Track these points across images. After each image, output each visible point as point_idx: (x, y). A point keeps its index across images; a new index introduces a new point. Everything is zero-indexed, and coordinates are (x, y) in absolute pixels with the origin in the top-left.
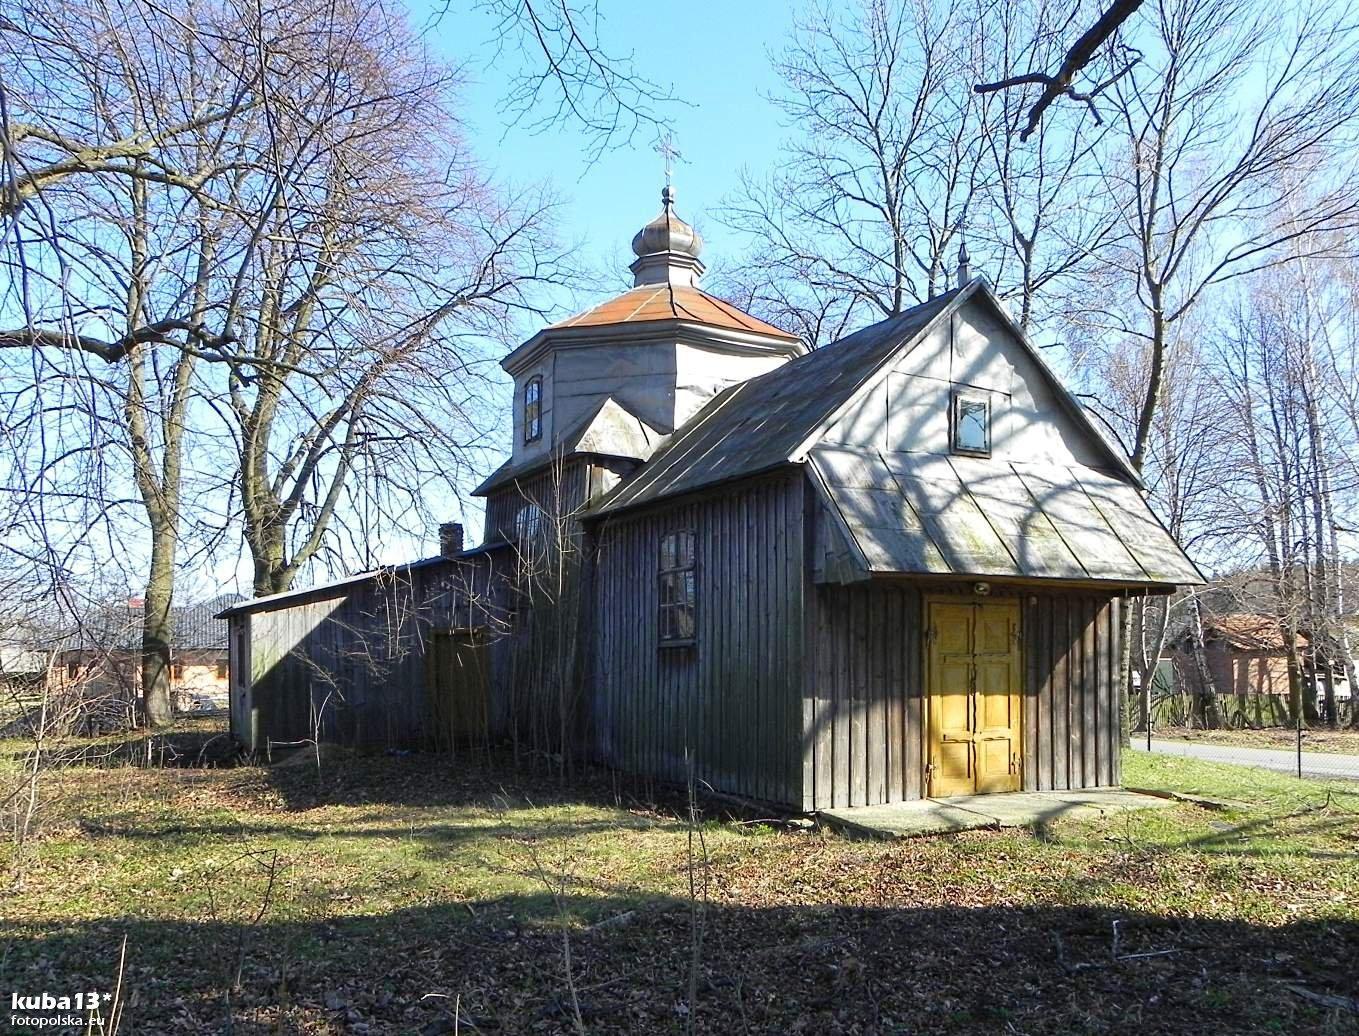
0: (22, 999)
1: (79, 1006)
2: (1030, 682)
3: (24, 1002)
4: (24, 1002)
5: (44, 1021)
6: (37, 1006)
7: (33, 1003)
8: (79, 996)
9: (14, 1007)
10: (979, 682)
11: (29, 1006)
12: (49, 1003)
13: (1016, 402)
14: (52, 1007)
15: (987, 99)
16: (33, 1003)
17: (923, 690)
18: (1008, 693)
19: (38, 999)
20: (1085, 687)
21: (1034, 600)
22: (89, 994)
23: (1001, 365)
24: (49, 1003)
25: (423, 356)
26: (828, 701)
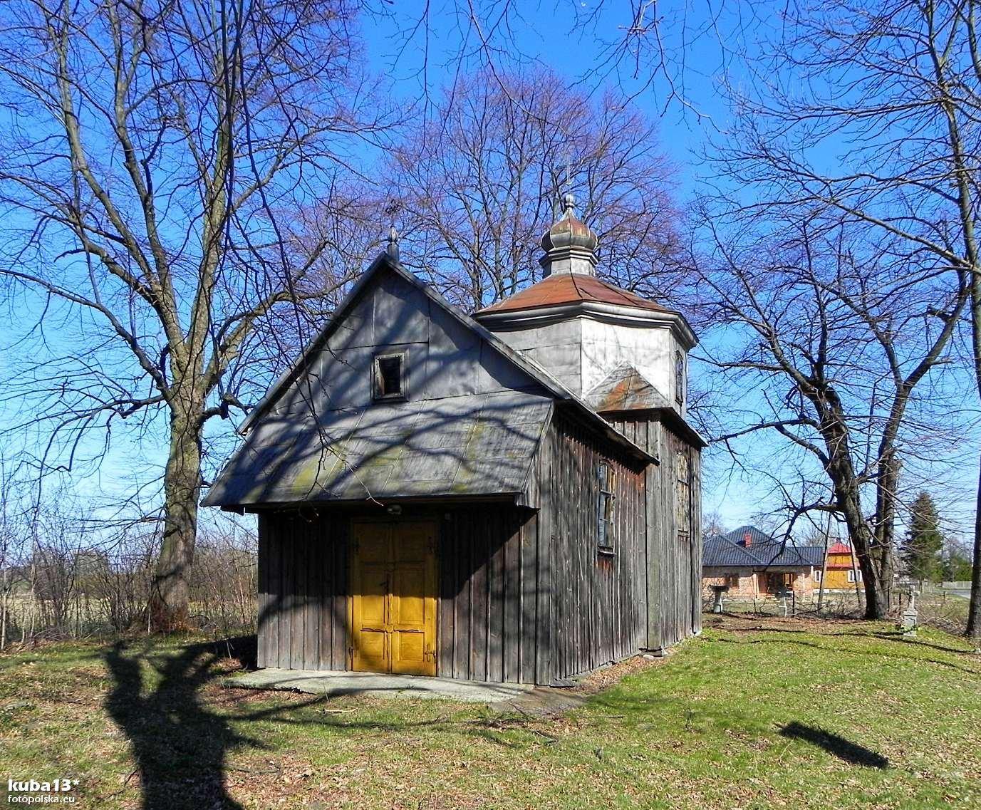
0: (16, 783)
1: (56, 789)
2: (447, 589)
3: (17, 786)
4: (17, 786)
5: (31, 800)
6: (26, 789)
7: (23, 786)
8: (56, 782)
9: (10, 789)
10: (390, 587)
11: (21, 789)
12: (35, 786)
13: (433, 350)
14: (37, 789)
15: (162, 5)
16: (23, 786)
17: (346, 591)
18: (436, 598)
19: (27, 784)
20: (507, 595)
21: (448, 516)
22: (64, 780)
23: (418, 323)
24: (35, 786)
25: (899, 489)
26: (276, 596)
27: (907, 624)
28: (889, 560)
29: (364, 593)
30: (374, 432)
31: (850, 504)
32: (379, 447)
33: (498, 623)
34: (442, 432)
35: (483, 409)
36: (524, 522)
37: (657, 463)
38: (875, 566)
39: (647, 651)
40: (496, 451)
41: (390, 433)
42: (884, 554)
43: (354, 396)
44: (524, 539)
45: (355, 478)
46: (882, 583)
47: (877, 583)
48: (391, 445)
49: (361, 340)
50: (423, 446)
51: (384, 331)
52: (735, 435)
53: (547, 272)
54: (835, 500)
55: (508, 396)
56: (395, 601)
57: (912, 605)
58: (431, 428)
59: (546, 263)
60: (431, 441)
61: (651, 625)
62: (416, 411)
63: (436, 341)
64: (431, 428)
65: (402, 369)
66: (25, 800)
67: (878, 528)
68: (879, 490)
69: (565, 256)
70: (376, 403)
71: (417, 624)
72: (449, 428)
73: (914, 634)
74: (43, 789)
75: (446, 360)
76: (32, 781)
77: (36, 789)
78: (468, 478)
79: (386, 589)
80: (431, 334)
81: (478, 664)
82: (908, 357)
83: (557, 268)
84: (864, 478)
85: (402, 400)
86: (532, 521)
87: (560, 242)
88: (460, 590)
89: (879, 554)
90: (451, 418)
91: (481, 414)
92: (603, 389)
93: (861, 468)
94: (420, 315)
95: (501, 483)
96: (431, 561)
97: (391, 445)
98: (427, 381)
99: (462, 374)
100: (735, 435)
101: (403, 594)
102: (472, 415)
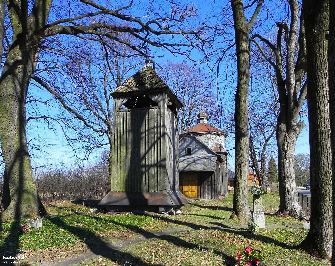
3: (6, 258)
4: (6, 258)
5: (11, 262)
9: (3, 259)
11: (7, 259)
12: (12, 258)
16: (8, 258)
19: (9, 257)
24: (12, 258)
27: (268, 191)
28: (264, 178)
29: (184, 185)
30: (188, 160)
31: (256, 166)
32: (190, 163)
33: (208, 189)
34: (200, 161)
35: (206, 157)
36: (212, 174)
37: (224, 162)
38: (261, 179)
39: (223, 196)
40: (210, 164)
41: (191, 160)
42: (263, 177)
43: (183, 154)
44: (213, 177)
45: (187, 168)
46: (263, 183)
47: (262, 183)
48: (192, 162)
49: (183, 145)
50: (198, 163)
51: (188, 143)
52: (230, 150)
53: (199, 122)
54: (252, 165)
55: (210, 155)
56: (191, 187)
57: (269, 187)
58: (198, 160)
59: (198, 120)
60: (199, 162)
61: (223, 191)
62: (194, 156)
63: (197, 146)
64: (198, 160)
65: (191, 150)
66: (9, 262)
67: (261, 171)
68: (262, 163)
69: (203, 119)
70: (186, 155)
71: (194, 190)
72: (201, 160)
73: (269, 193)
74: (15, 259)
75: (199, 149)
76: (11, 256)
77: (12, 259)
78: (207, 168)
79: (189, 185)
80: (196, 145)
81: (205, 196)
82: (267, 136)
83: (201, 122)
84: (259, 161)
85: (191, 155)
86: (214, 174)
87: (202, 117)
88: (202, 185)
89: (262, 176)
90: (201, 158)
91: (206, 158)
92: (213, 147)
93: (258, 159)
94: (194, 142)
95: (212, 169)
96: (196, 180)
97: (192, 162)
98: (196, 152)
99: (202, 151)
100: (230, 150)
101: (192, 185)
102: (204, 158)
